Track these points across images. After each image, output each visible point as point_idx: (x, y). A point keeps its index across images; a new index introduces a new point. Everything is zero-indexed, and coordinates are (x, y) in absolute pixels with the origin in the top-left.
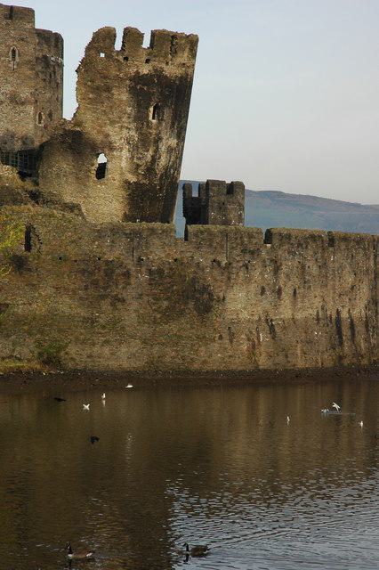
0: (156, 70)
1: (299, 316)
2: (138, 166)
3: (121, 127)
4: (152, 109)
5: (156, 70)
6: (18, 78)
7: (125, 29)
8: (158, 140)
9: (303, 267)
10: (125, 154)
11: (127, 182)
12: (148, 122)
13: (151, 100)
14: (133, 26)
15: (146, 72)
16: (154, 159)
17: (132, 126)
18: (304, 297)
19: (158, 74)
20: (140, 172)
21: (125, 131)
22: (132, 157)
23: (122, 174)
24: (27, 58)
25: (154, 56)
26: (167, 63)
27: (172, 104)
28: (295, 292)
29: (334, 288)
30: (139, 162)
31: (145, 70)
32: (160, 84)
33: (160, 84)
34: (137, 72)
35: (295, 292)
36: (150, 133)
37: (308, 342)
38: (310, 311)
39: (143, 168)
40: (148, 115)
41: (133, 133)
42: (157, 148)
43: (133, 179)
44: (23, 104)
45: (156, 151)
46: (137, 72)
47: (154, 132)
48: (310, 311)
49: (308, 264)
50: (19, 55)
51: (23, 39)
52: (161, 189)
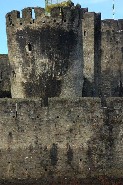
0: (25, 27)
1: (14, 147)
2: (26, 74)
3: (17, 57)
4: (27, 46)
5: (25, 27)
6: (87, 43)
7: (22, 10)
8: (34, 60)
9: (17, 120)
10: (20, 70)
11: (23, 83)
12: (26, 53)
13: (26, 42)
14: (10, 11)
15: (21, 29)
16: (33, 71)
17: (20, 56)
18: (18, 136)
19: (27, 29)
20: (27, 77)
21: (18, 59)
22: (23, 70)
23: (20, 79)
24: (90, 34)
25: (23, 21)
26: (31, 23)
27: (38, 42)
28: (10, 134)
29: (49, 131)
30: (26, 72)
31: (21, 28)
32: (28, 34)
33: (28, 34)
34: (18, 30)
35: (10, 134)
36: (29, 58)
37: (18, 163)
38: (24, 145)
39: (28, 75)
40: (26, 50)
41: (21, 59)
42: (34, 64)
43: (25, 81)
44: (89, 53)
45: (34, 65)
46: (18, 30)
47: (30, 57)
48: (24, 145)
49: (21, 118)
50: (87, 33)
51: (88, 26)
52: (42, 84)
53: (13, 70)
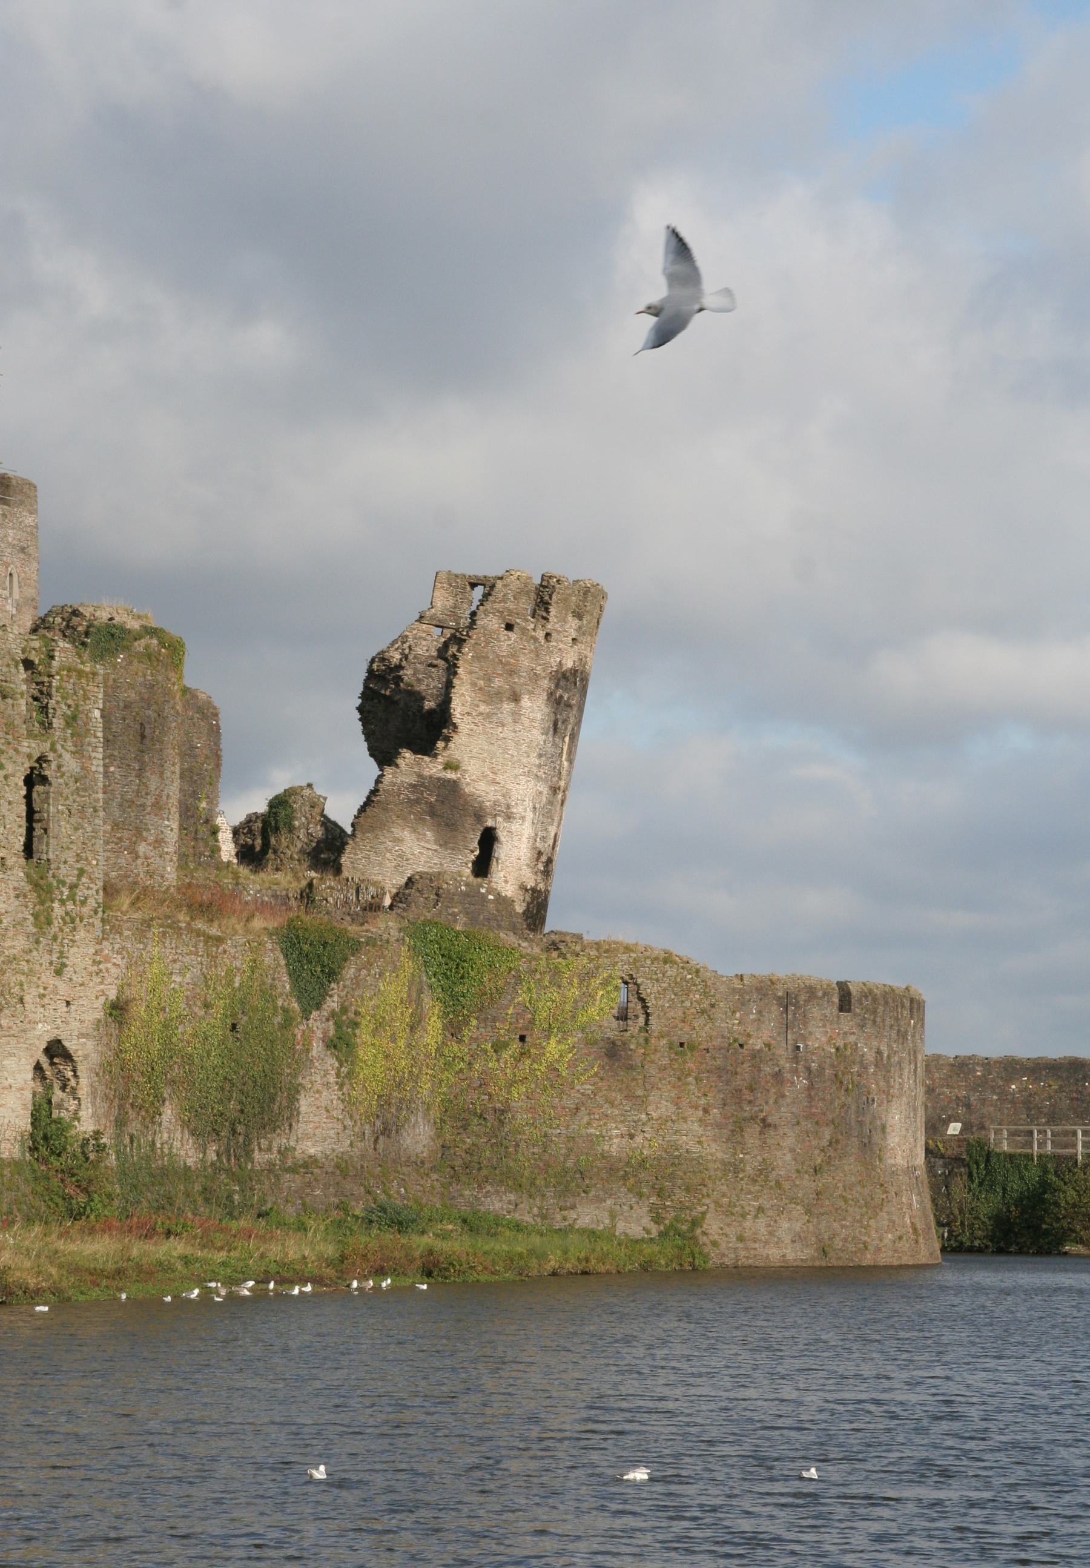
53: (490, 823)
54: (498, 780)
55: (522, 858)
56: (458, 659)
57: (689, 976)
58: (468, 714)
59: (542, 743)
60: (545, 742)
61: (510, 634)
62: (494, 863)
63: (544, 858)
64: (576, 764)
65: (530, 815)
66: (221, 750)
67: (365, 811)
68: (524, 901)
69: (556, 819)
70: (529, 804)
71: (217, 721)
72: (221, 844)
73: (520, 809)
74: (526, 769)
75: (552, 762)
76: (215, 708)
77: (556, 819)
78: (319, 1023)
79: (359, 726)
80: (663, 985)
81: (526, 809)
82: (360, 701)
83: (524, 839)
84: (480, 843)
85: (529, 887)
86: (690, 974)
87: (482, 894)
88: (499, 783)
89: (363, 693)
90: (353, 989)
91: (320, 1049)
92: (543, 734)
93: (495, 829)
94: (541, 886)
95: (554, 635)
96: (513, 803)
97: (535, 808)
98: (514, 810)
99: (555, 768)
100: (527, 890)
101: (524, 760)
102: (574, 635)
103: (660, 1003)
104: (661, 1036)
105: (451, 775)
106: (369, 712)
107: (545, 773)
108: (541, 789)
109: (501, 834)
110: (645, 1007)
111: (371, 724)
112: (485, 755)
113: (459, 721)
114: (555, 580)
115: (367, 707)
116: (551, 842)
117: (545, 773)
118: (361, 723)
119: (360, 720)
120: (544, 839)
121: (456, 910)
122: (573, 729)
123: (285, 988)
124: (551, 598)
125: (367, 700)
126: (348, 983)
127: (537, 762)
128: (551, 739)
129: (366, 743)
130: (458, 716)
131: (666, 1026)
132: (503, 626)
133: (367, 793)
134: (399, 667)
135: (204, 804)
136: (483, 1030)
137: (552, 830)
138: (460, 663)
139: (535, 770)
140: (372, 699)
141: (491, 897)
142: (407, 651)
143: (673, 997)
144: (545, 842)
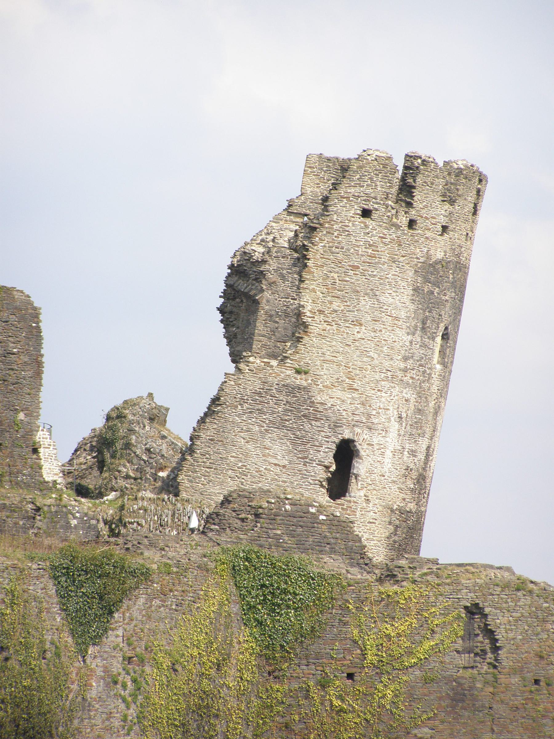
53: (347, 435)
54: (355, 386)
55: (387, 474)
56: (307, 250)
57: (546, 605)
58: (321, 312)
59: (408, 344)
60: (411, 342)
61: (367, 221)
62: (353, 480)
63: (414, 475)
64: (455, 368)
65: (394, 426)
66: (42, 356)
67: (204, 422)
68: (390, 523)
69: (428, 431)
70: (393, 413)
71: (37, 323)
72: (42, 462)
73: (383, 418)
74: (389, 373)
75: (421, 365)
76: (35, 309)
77: (428, 431)
78: (98, 660)
79: (220, 329)
80: (514, 614)
81: (389, 419)
82: (222, 300)
83: (389, 454)
84: (335, 457)
85: (395, 507)
86: (547, 602)
87: (312, 514)
88: (357, 390)
89: (225, 292)
90: (142, 622)
91: (100, 689)
92: (408, 334)
93: (353, 441)
94: (412, 506)
95: (419, 221)
96: (374, 412)
97: (400, 417)
98: (376, 421)
99: (424, 372)
100: (392, 511)
101: (387, 364)
102: (443, 220)
103: (511, 635)
104: (514, 671)
105: (301, 381)
106: (231, 312)
107: (412, 378)
108: (408, 396)
109: (362, 448)
110: (494, 641)
111: (233, 326)
112: (340, 358)
113: (310, 320)
114: (419, 161)
115: (229, 308)
116: (421, 456)
117: (412, 378)
118: (222, 325)
119: (222, 321)
120: (413, 453)
121: (279, 532)
122: (446, 328)
123: (55, 619)
124: (414, 181)
125: (228, 299)
126: (136, 614)
127: (402, 365)
128: (419, 339)
129: (228, 348)
130: (308, 314)
131: (519, 662)
132: (359, 212)
133: (207, 402)
134: (264, 262)
135: (21, 416)
136: (305, 667)
137: (424, 443)
138: (310, 255)
139: (400, 374)
140: (234, 299)
141: (322, 517)
142: (271, 244)
143: (526, 627)
144: (415, 456)
